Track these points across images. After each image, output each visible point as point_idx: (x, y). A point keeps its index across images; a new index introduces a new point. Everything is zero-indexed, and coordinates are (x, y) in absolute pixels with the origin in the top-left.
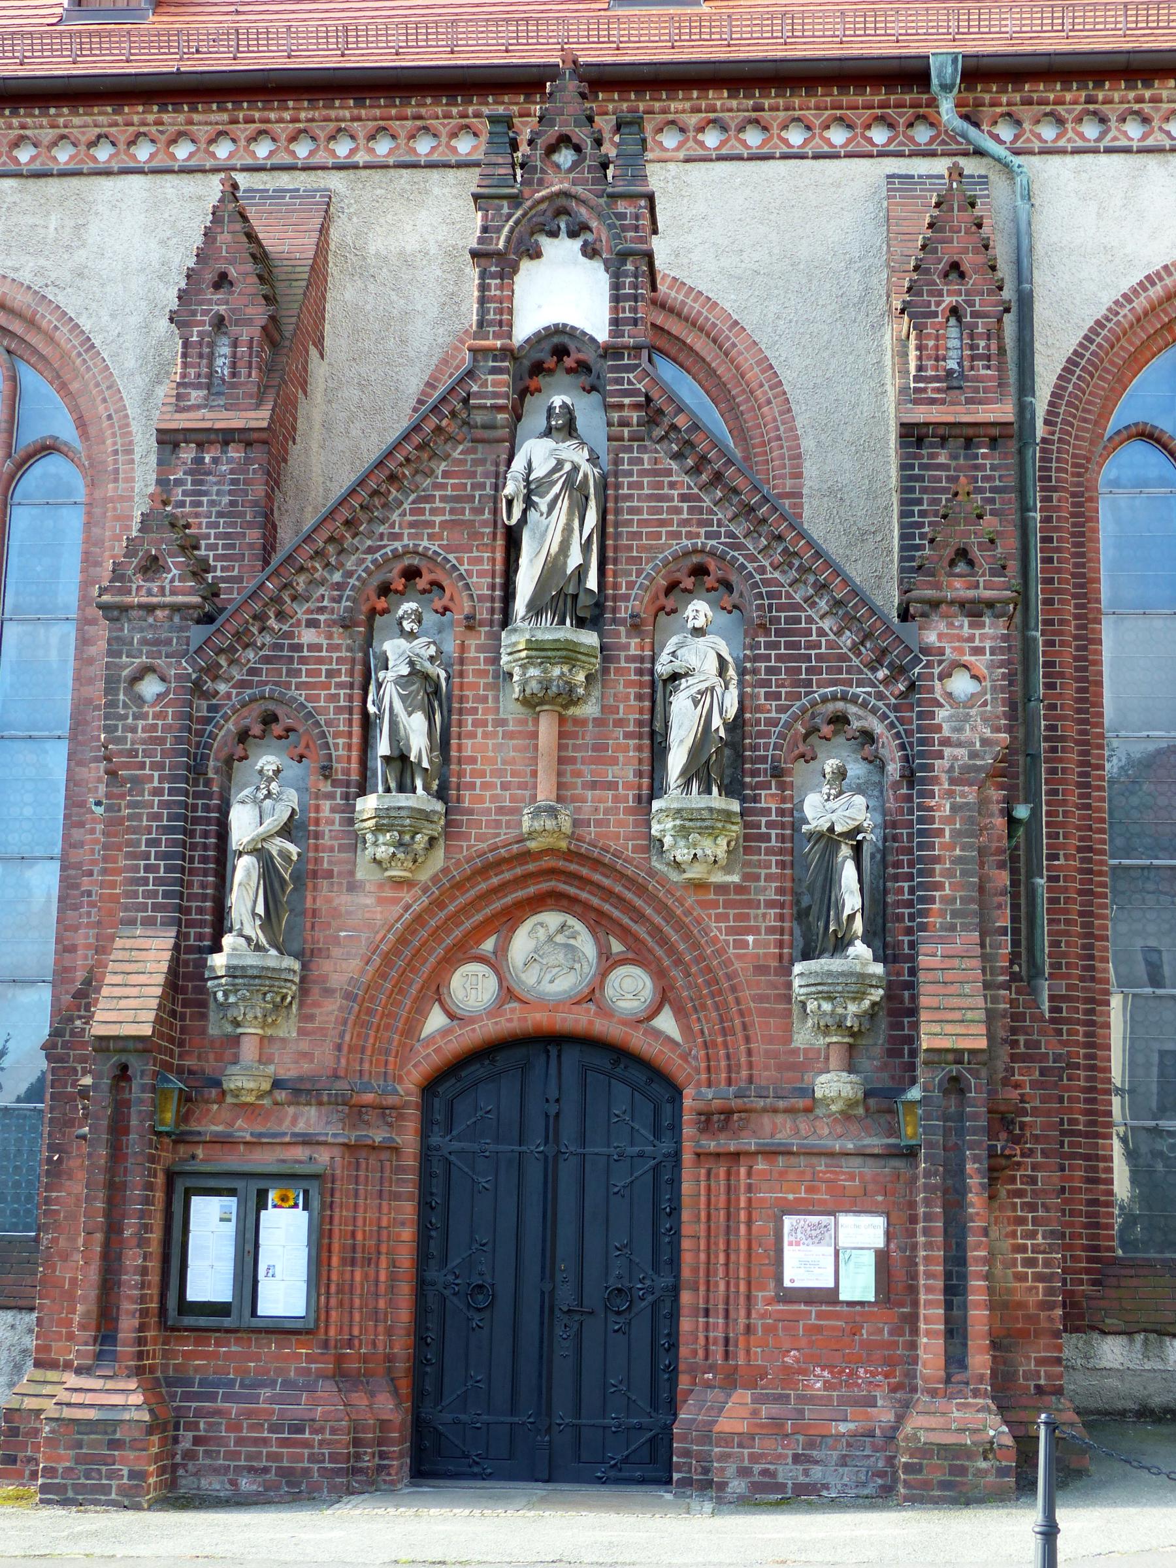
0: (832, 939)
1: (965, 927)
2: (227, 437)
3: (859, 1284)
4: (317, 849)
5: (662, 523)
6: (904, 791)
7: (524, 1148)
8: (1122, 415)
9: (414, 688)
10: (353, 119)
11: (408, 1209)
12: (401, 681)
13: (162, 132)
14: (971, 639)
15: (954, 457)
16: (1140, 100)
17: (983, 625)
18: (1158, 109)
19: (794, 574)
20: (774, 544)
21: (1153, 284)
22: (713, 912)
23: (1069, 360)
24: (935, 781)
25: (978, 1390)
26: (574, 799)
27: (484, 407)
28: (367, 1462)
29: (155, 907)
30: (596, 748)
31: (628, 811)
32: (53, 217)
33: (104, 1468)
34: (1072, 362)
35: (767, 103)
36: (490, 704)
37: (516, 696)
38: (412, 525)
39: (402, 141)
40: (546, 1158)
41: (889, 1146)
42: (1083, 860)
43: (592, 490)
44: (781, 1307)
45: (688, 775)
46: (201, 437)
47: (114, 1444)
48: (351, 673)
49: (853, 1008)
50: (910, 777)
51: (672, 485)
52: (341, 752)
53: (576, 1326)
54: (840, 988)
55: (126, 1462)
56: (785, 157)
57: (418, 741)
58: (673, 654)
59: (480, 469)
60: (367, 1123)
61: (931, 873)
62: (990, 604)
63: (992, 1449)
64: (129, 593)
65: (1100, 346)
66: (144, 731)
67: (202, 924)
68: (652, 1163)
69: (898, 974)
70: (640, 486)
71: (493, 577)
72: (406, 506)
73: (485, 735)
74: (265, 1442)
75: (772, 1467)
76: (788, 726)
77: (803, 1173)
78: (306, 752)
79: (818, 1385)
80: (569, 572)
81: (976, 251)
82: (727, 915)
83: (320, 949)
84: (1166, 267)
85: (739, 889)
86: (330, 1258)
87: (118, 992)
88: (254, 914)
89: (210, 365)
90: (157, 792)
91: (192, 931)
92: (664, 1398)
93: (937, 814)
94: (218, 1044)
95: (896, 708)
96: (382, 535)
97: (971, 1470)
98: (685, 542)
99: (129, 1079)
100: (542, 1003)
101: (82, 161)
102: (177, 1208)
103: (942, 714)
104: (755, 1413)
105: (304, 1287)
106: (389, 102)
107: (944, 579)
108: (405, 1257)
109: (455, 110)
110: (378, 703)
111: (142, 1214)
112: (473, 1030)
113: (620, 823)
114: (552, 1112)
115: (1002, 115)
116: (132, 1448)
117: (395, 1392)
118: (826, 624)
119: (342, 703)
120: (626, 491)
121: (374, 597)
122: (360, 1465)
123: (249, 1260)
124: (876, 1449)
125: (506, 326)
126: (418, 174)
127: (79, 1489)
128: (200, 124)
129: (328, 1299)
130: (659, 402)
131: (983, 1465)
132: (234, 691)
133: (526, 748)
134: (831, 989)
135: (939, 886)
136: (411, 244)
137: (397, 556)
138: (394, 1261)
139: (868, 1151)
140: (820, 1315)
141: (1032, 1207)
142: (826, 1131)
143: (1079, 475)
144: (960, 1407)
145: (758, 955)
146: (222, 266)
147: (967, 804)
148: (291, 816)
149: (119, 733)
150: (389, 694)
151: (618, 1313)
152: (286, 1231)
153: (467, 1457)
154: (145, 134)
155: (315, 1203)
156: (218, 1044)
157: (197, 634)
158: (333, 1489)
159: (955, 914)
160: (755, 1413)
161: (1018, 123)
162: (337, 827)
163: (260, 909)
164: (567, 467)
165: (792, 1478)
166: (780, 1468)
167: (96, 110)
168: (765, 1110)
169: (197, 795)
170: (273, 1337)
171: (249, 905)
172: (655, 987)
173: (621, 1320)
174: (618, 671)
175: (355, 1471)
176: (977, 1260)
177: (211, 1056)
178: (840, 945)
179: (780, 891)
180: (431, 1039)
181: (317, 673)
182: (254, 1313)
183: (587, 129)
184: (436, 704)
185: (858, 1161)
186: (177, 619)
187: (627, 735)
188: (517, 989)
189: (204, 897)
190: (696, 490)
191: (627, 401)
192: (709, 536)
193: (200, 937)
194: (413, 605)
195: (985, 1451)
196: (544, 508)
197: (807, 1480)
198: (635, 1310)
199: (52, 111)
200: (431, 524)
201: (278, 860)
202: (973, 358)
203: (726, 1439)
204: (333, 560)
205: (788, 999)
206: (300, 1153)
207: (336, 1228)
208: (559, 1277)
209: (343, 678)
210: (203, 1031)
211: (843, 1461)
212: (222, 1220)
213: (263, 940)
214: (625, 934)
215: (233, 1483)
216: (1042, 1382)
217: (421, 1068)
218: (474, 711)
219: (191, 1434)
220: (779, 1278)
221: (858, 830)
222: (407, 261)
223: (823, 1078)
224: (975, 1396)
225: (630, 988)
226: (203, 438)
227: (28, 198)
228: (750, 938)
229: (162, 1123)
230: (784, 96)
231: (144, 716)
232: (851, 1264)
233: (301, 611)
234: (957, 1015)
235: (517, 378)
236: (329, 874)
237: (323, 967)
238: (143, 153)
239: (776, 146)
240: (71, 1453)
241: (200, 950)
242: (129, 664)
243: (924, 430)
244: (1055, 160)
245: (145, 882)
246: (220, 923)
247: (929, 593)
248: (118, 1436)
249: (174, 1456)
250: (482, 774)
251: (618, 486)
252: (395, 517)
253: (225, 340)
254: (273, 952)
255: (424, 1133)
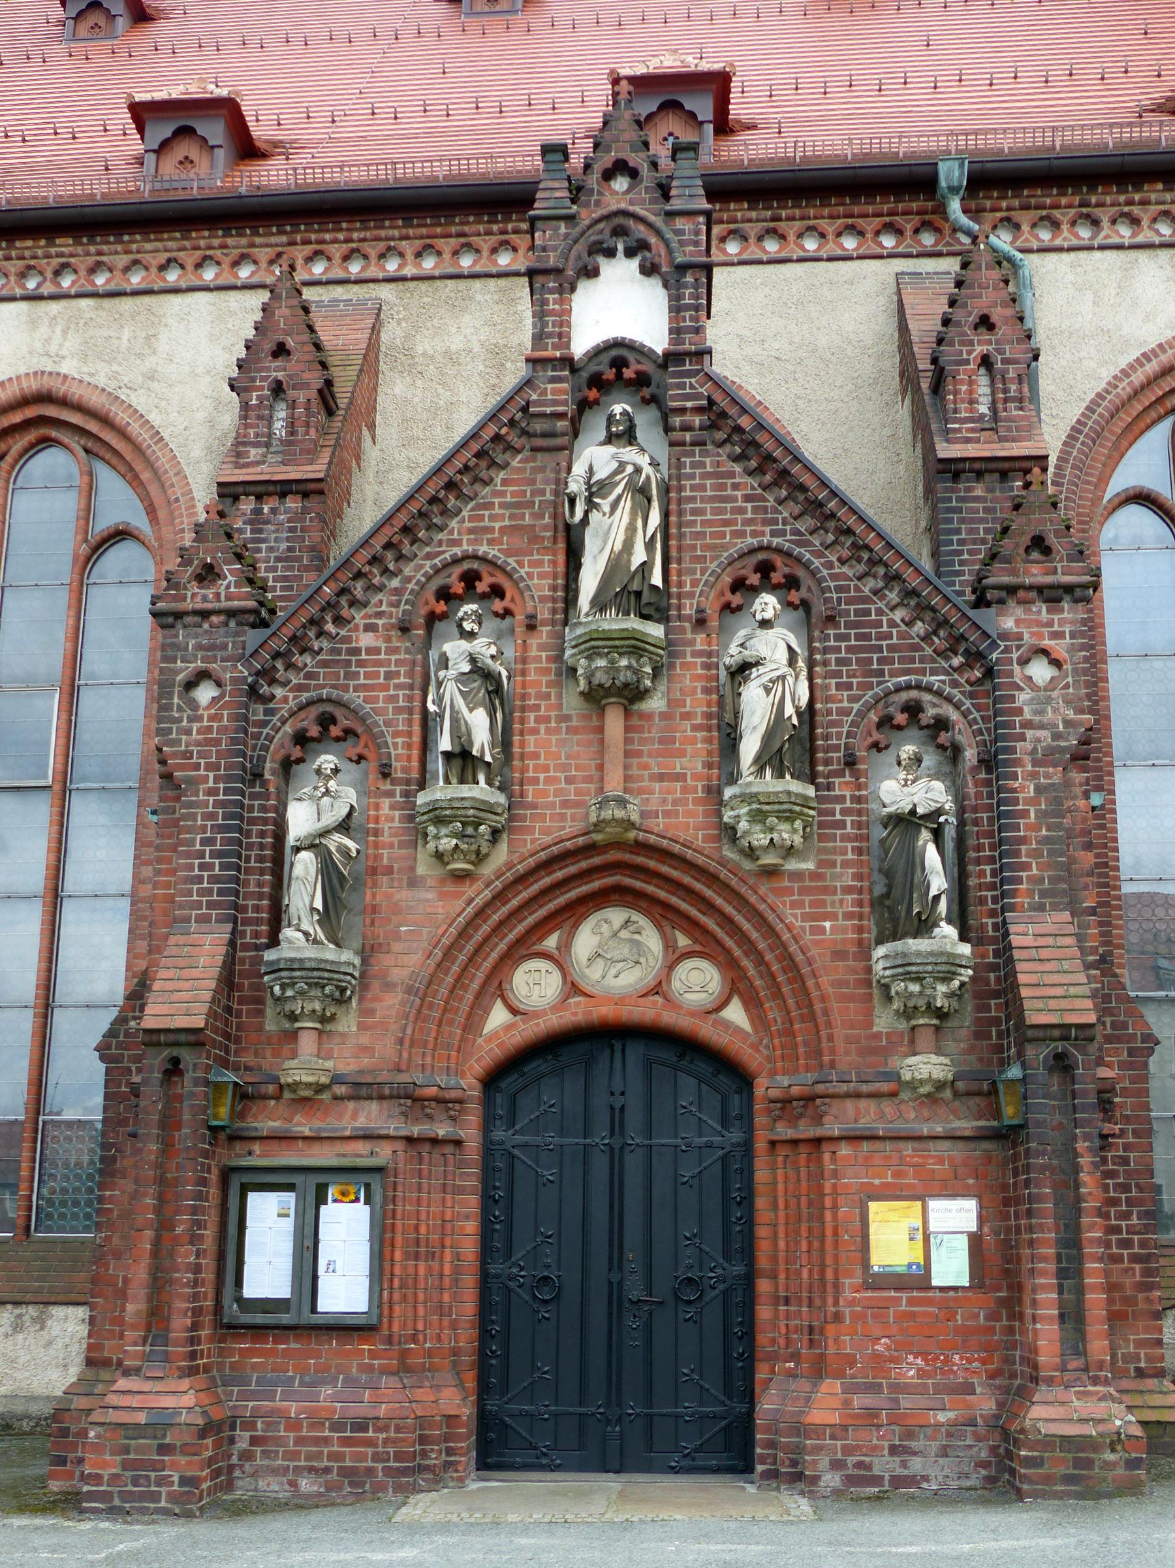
0: (916, 922)
1: (1055, 907)
2: (284, 489)
3: (952, 1268)
4: (376, 845)
5: (726, 523)
6: (983, 776)
7: (588, 1141)
8: (1123, 479)
9: (476, 685)
10: (402, 238)
11: (473, 1201)
12: (462, 678)
13: (226, 255)
14: (1050, 623)
15: (990, 490)
16: (1130, 203)
17: (1062, 611)
18: (1146, 211)
19: (862, 568)
20: (843, 539)
21: (1149, 360)
22: (787, 899)
23: (1073, 428)
24: (1018, 762)
25: (1097, 1377)
26: (641, 791)
27: (543, 415)
28: (433, 1460)
29: (211, 905)
30: (662, 741)
31: (696, 801)
32: (126, 330)
33: (153, 1474)
34: (1076, 430)
35: (784, 214)
36: (553, 700)
37: (581, 689)
38: (471, 531)
39: (447, 256)
40: (612, 1149)
41: (979, 1128)
42: (1100, 875)
43: (654, 492)
44: (869, 1294)
45: (760, 763)
46: (260, 489)
47: (164, 1449)
48: (410, 674)
49: (942, 988)
50: (989, 762)
51: (735, 487)
52: (400, 751)
53: (646, 1315)
54: (930, 968)
55: (176, 1469)
56: (801, 260)
57: (480, 727)
58: (742, 645)
59: (539, 477)
60: (431, 1117)
61: (1017, 854)
62: (1069, 589)
63: (1119, 1440)
64: (184, 599)
65: (1101, 415)
66: (198, 732)
67: (258, 921)
68: (721, 1153)
69: (983, 956)
70: (702, 488)
71: (555, 578)
72: (465, 513)
73: (548, 731)
74: (326, 1441)
75: (867, 1459)
76: (862, 714)
77: (889, 1157)
78: (365, 752)
79: (911, 1373)
80: (633, 568)
81: (1004, 305)
82: (803, 902)
83: (380, 945)
84: (1160, 346)
85: (814, 876)
86: (393, 1252)
87: (170, 985)
88: (313, 909)
89: (270, 426)
90: (212, 792)
91: (248, 929)
92: (742, 1389)
93: (1021, 795)
94: (275, 1040)
95: (972, 695)
96: (440, 543)
97: (1097, 1463)
98: (749, 540)
99: (180, 1073)
100: (609, 1000)
101: (153, 281)
102: (233, 1204)
103: (1022, 698)
104: (847, 1404)
105: (366, 1282)
106: (434, 221)
107: (1020, 566)
108: (470, 1249)
109: (495, 227)
110: (439, 701)
111: (194, 1210)
112: (538, 1024)
113: (689, 814)
114: (617, 1106)
115: (1002, 220)
116: (183, 1453)
117: (461, 1385)
118: (898, 615)
119: (401, 704)
120: (688, 493)
121: (433, 600)
122: (427, 1462)
123: (308, 1255)
124: (978, 1438)
125: (564, 338)
126: (462, 284)
127: (126, 1496)
128: (261, 246)
129: (391, 1294)
130: (723, 403)
131: (1111, 1457)
132: (291, 695)
133: (590, 743)
134: (920, 968)
135: (1026, 867)
136: (457, 343)
137: (456, 561)
138: (458, 1254)
139: (959, 1134)
140: (911, 1302)
141: (1125, 1188)
142: (913, 1115)
143: (1084, 531)
144: (1081, 1395)
145: (835, 941)
146: (281, 338)
147: (1053, 785)
148: (349, 815)
149: (174, 736)
150: (452, 691)
151: (689, 1302)
152: (346, 1226)
153: (536, 1448)
154: (211, 258)
155: (377, 1197)
156: (275, 1040)
157: (253, 637)
158: (399, 1489)
159: (1043, 894)
160: (847, 1404)
161: (1017, 226)
162: (397, 824)
163: (318, 904)
164: (630, 469)
165: (888, 1470)
166: (876, 1460)
167: (166, 236)
168: (848, 1095)
169: (253, 796)
170: (334, 1334)
171: (307, 900)
172: (724, 978)
173: (692, 1310)
174: (685, 666)
175: (422, 1469)
176: (1091, 1241)
177: (268, 1053)
178: (924, 926)
179: (859, 877)
180: (495, 1034)
181: (376, 675)
182: (314, 1309)
183: (643, 155)
184: (497, 702)
185: (947, 1144)
186: (232, 624)
187: (695, 728)
188: (583, 985)
189: (260, 896)
190: (760, 491)
191: (689, 404)
192: (773, 534)
193: (256, 935)
194: (474, 607)
195: (1112, 1443)
196: (606, 508)
197: (906, 1472)
198: (707, 1299)
199: (126, 238)
200: (491, 530)
201: (336, 856)
202: (1006, 400)
203: (817, 1431)
204: (391, 566)
205: (868, 984)
206: (361, 1147)
207: (399, 1223)
208: (628, 1267)
209: (402, 680)
210: (260, 1028)
211: (944, 1452)
212: (279, 1215)
213: (321, 936)
214: (692, 926)
215: (293, 1484)
216: (1142, 1365)
217: (483, 1063)
218: (537, 708)
219: (247, 1434)
220: (866, 1263)
221: (939, 812)
222: (452, 358)
223: (911, 1060)
224: (1095, 1384)
225: (698, 981)
226: (262, 490)
227: (104, 314)
228: (827, 924)
229: (216, 1117)
230: (800, 207)
231: (200, 719)
232: (943, 1249)
233: (359, 617)
234: (1059, 991)
235: (576, 389)
236: (389, 871)
237: (383, 961)
238: (209, 275)
239: (793, 251)
240: (118, 1458)
241: (257, 948)
242: (184, 670)
243: (961, 466)
244: (1054, 257)
245: (200, 880)
246: (277, 917)
247: (1006, 579)
248: (167, 1441)
249: (230, 1456)
250: (546, 769)
251: (680, 489)
252: (454, 523)
253: (283, 405)
254: (332, 946)
255: (487, 1126)
